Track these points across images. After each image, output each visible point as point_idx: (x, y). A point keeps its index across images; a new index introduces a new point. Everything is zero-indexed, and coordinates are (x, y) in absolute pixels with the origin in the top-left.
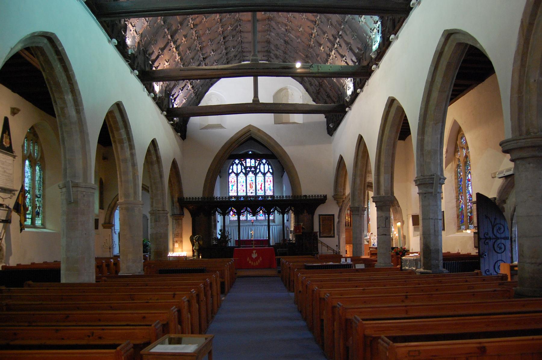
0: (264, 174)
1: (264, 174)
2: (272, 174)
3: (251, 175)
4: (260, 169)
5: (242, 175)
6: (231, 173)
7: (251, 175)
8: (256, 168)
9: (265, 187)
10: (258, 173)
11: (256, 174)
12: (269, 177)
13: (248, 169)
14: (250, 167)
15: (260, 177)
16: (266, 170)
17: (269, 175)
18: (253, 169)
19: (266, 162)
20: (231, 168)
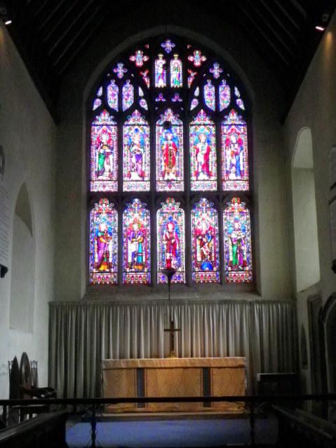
0: (217, 117)
2: (245, 116)
3: (169, 116)
4: (201, 98)
6: (99, 112)
8: (186, 93)
9: (219, 162)
12: (235, 129)
13: (160, 99)
14: (168, 91)
15: (202, 129)
16: (225, 103)
17: (233, 118)
19: (222, 76)
20: (100, 93)
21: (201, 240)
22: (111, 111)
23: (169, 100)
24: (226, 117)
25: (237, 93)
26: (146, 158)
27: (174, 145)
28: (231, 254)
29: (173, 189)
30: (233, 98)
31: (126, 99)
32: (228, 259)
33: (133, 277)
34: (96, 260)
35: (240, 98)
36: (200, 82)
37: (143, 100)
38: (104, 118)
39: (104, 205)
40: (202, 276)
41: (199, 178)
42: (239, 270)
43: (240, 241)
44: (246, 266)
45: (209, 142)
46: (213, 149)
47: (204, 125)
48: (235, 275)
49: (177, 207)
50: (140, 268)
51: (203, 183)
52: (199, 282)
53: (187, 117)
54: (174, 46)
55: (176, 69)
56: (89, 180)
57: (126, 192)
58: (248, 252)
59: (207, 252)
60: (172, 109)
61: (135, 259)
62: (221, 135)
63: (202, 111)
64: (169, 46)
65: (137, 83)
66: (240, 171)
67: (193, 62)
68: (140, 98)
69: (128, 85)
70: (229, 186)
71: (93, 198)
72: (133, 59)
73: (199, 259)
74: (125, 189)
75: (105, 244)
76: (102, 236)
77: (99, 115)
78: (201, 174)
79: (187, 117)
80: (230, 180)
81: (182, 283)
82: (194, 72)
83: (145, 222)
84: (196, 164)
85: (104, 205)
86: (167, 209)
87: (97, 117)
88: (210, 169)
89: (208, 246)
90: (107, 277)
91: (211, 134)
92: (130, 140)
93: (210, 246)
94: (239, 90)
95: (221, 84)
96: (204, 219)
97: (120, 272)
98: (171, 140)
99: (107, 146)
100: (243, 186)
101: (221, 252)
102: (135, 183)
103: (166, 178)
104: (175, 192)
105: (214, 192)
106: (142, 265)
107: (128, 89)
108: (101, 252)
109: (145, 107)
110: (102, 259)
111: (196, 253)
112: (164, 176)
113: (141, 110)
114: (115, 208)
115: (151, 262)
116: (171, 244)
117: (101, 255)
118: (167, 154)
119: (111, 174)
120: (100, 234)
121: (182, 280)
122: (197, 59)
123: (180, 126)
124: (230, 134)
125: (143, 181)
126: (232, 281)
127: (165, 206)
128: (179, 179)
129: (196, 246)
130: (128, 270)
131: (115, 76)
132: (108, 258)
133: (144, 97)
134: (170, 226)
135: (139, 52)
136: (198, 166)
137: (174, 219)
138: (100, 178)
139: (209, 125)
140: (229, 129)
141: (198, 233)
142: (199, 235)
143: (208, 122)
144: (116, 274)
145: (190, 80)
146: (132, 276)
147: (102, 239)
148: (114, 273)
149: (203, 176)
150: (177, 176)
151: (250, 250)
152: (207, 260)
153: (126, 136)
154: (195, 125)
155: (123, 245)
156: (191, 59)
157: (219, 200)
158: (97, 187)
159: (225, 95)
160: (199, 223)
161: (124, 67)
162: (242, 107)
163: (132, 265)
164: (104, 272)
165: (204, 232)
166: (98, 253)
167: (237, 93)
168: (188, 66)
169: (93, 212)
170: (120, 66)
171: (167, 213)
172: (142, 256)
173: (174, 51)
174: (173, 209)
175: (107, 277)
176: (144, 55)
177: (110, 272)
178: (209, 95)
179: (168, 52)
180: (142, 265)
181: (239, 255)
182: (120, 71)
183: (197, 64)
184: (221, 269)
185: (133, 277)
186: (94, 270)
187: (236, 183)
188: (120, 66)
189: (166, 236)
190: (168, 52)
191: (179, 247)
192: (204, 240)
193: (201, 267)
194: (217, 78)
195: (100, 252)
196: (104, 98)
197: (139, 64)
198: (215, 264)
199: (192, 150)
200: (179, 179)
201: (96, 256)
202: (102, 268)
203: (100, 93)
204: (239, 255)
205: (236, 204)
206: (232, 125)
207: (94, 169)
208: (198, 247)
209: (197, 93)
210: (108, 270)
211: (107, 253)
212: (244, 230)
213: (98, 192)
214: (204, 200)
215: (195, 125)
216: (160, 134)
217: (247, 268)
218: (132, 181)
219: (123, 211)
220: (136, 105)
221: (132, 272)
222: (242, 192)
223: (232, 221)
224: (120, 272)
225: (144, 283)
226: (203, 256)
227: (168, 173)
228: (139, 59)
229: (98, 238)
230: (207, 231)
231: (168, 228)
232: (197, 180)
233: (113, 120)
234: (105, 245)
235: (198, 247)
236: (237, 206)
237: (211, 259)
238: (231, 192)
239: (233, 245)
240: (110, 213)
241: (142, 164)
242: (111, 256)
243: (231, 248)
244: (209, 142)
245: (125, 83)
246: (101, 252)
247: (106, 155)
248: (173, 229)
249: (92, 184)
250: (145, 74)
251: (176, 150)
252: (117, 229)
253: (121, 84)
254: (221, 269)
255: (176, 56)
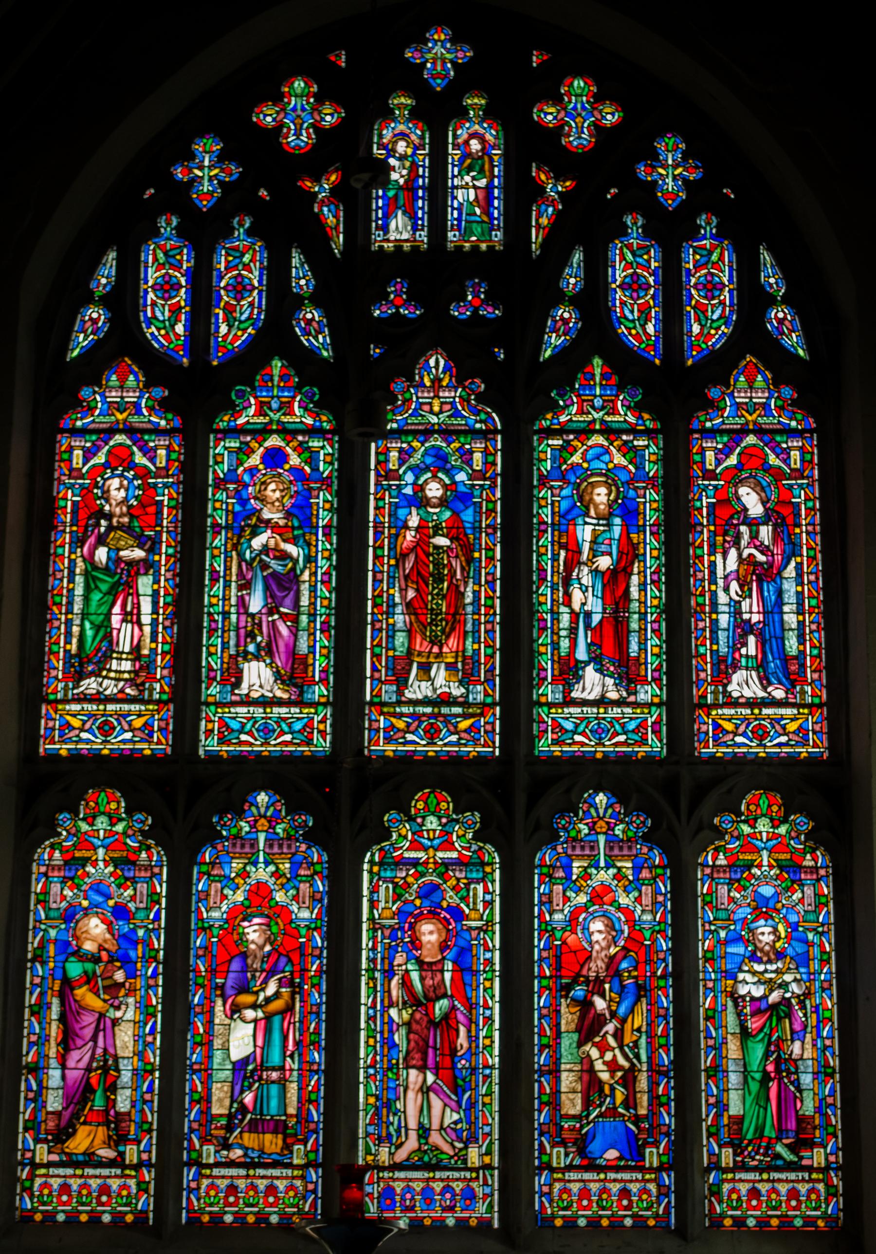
0: (674, 392)
1: (674, 392)
2: (812, 386)
3: (435, 395)
4: (594, 300)
5: (277, 412)
6: (93, 368)
7: (435, 395)
8: (521, 278)
9: (678, 615)
10: (569, 367)
11: (519, 394)
12: (759, 451)
13: (395, 304)
14: (434, 268)
15: (597, 445)
16: (709, 325)
17: (751, 394)
18: (471, 304)
19: (698, 196)
20: (105, 276)
21: (586, 1005)
22: (155, 367)
23: (436, 311)
24: (714, 393)
25: (771, 278)
26: (315, 594)
27: (455, 530)
28: (734, 1079)
29: (447, 743)
30: (752, 300)
31: (229, 309)
32: (722, 1106)
33: (232, 1189)
34: (54, 1102)
35: (785, 300)
36: (589, 227)
37: (312, 314)
38: (123, 393)
39: (102, 823)
40: (585, 1193)
41: (409, 694)
42: (775, 1165)
43: (781, 1010)
44: (811, 1145)
45: (630, 514)
46: (651, 546)
47: (608, 431)
48: (754, 1193)
49: (462, 840)
50: (272, 1143)
51: (594, 710)
52: (570, 1223)
53: (519, 394)
54: (466, 54)
55: (472, 163)
56: (32, 697)
57: (214, 758)
58: (822, 1072)
59: (612, 1066)
60: (450, 357)
61: (248, 1098)
62: (689, 481)
63: (277, 365)
64: (439, 54)
65: (286, 226)
66: (785, 659)
67: (559, 130)
68: (298, 302)
69: (240, 237)
70: (726, 736)
71: (54, 787)
72: (267, 116)
73: (572, 1104)
74: (209, 744)
75: (102, 1016)
76: (88, 979)
77: (95, 380)
78: (590, 674)
79: (519, 394)
80: (733, 703)
81: (484, 1224)
82: (559, 177)
83: (644, 906)
84: (565, 620)
85: (102, 823)
86: (415, 846)
87: (85, 393)
88: (634, 648)
89: (618, 1035)
90: (104, 1189)
91: (640, 475)
92: (243, 502)
93: (628, 1039)
94: (781, 262)
95: (693, 233)
96: (600, 895)
97: (169, 1166)
98: (443, 502)
99: (128, 529)
100: (794, 730)
101: (685, 1071)
102: (259, 705)
103: (418, 689)
104: (456, 760)
105: (649, 760)
106: (278, 1127)
107: (242, 262)
108: (79, 1058)
109: (321, 343)
110: (78, 1096)
111: (555, 1072)
112: (401, 682)
113: (303, 362)
114: (158, 833)
115: (327, 1114)
116: (433, 1024)
117: (74, 1075)
118: (424, 569)
119: (143, 667)
120: (75, 969)
121: (481, 1208)
122: (579, 114)
123: (486, 435)
124: (734, 477)
125: (300, 703)
126: (739, 1222)
127: (406, 828)
128: (478, 694)
129: (558, 1034)
130: (209, 1153)
131: (178, 198)
132: (112, 1088)
133: (316, 300)
134: (429, 933)
135: (299, 85)
136: (573, 631)
137: (451, 898)
138: (90, 685)
139: (633, 430)
140: (727, 451)
141: (570, 963)
142: (575, 981)
143: (623, 416)
144: (148, 1175)
145: (543, 218)
146: (229, 1187)
147: (82, 992)
148: (137, 1167)
149: (593, 683)
150: (468, 679)
151: (155, 1059)
152: (612, 1112)
153: (219, 484)
154: (562, 431)
155: (188, 1024)
156: (549, 115)
157: (678, 799)
158: (73, 728)
159: (711, 288)
160: (573, 919)
161: (222, 158)
162: (794, 341)
163: (229, 1128)
164: (90, 1160)
165: (597, 966)
166: (63, 1067)
167: (771, 278)
168: (529, 147)
169: (49, 855)
170: (207, 149)
171: (415, 863)
172: (283, 1083)
173: (465, 78)
174: (448, 845)
175: (104, 1189)
176: (320, 98)
177: (118, 1162)
178: (634, 285)
179: (438, 84)
180: (278, 1127)
181: (773, 1086)
182: (206, 171)
183: (579, 137)
184: (683, 1159)
185: (232, 1189)
186: (42, 1153)
187: (760, 712)
188: (207, 149)
189: (406, 983)
190: (438, 84)
191: (472, 1039)
192: (600, 1004)
193: (582, 1144)
194: (205, 204)
195: (75, 1055)
196: (124, 300)
197: (299, 139)
198: (655, 1129)
199: (546, 552)
200: (478, 694)
201: (54, 1076)
202: (81, 1141)
203: (105, 276)
204: (773, 1086)
205: (763, 826)
206: (744, 431)
207: (62, 646)
208: (568, 1042)
209: (572, 280)
210: (106, 1153)
211: (108, 1066)
212: (803, 960)
213: (76, 757)
214: (601, 799)
215: (562, 431)
216: (391, 475)
217: (818, 1157)
218: (247, 701)
219: (197, 849)
220: (275, 334)
221: (231, 1164)
222: (792, 761)
223: (744, 912)
224: (169, 1166)
225: (285, 1225)
226: (591, 1086)
227: (425, 668)
228: (298, 115)
229: (68, 985)
230: (612, 961)
231: (416, 943)
232: (569, 702)
233: (164, 406)
234: (105, 1026)
235: (568, 1042)
236: (763, 827)
237: (630, 1102)
238: (739, 763)
239: (745, 1034)
240: (132, 862)
241: (296, 620)
242: (126, 1077)
243: (733, 1048)
244: (630, 514)
245: (228, 232)
246: (79, 1058)
247: (123, 579)
248: (443, 947)
249: (49, 720)
250: (323, 188)
251: (467, 550)
252: (159, 943)
253: (204, 232)
254: (683, 1159)
255: (475, 101)
